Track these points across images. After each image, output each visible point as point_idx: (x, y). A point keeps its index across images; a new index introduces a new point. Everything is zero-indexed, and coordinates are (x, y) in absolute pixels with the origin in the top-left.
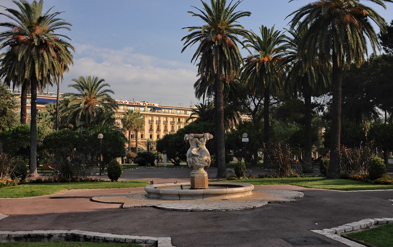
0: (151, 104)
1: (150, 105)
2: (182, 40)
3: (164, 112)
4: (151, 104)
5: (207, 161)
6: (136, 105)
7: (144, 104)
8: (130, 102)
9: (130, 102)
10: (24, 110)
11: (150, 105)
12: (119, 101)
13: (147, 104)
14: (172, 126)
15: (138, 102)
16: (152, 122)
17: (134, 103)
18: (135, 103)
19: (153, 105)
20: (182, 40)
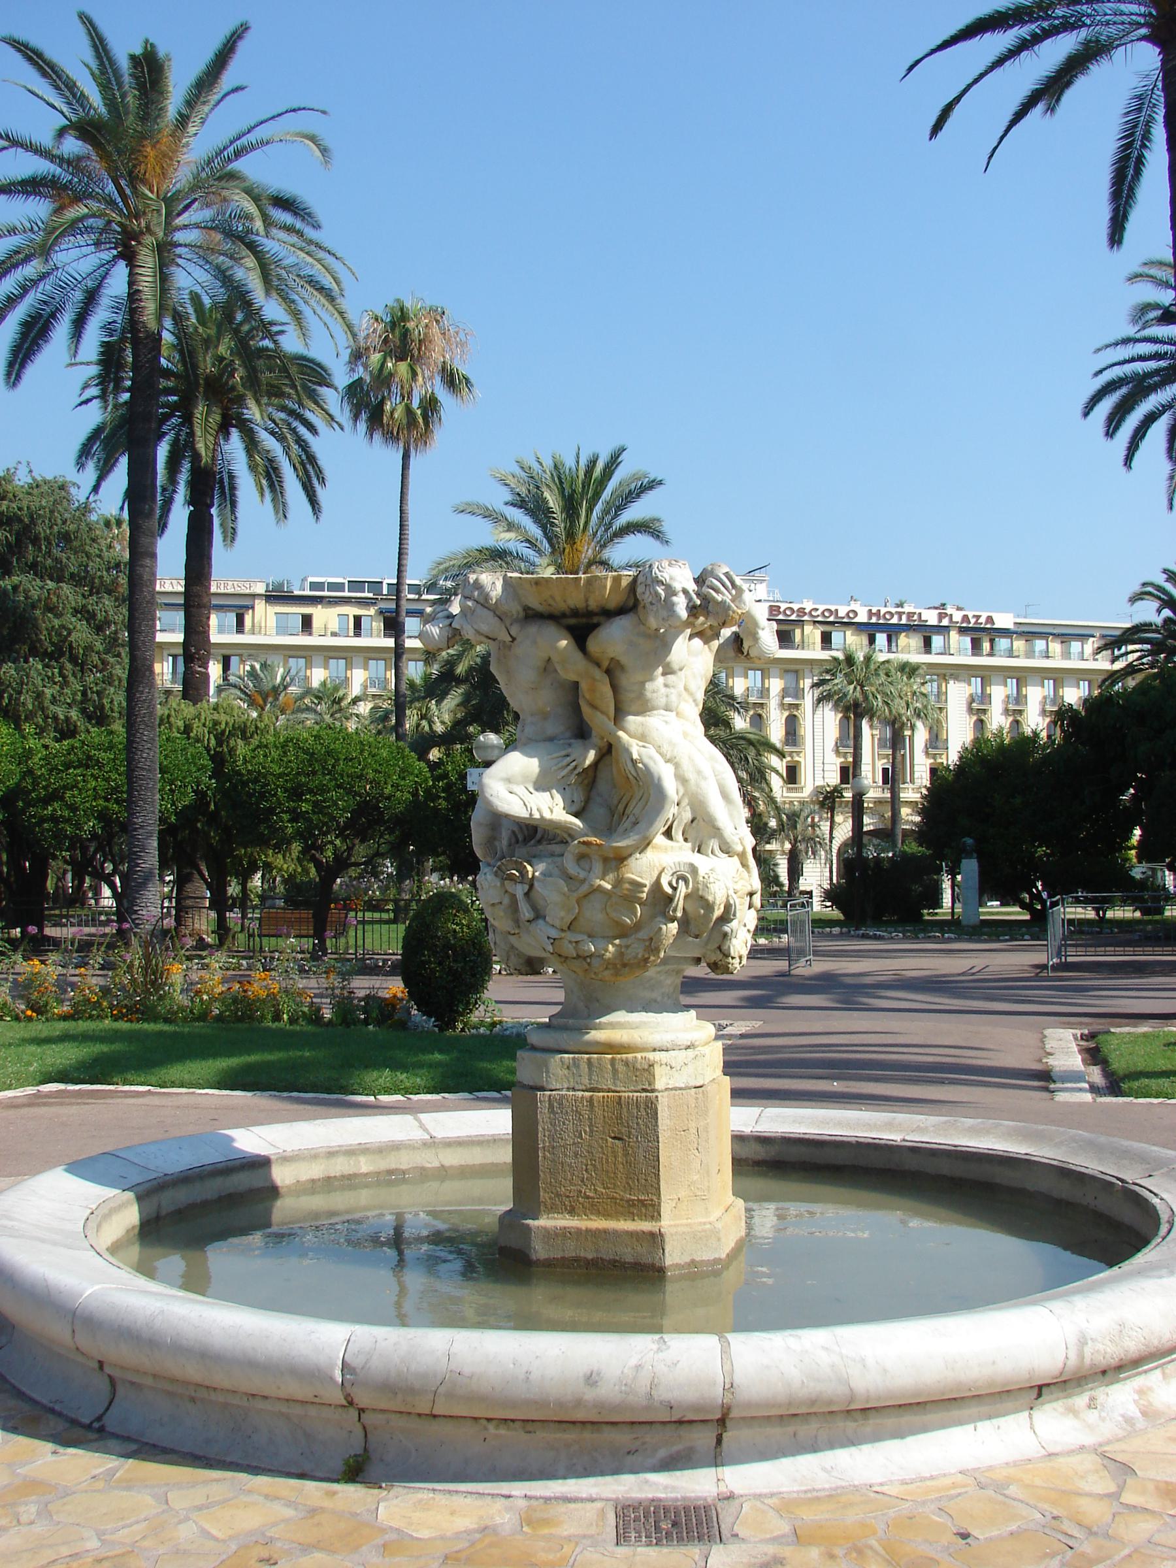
0: (978, 617)
1: (973, 621)
2: (1088, 410)
3: (1011, 654)
4: (978, 617)
5: (670, 899)
6: (904, 621)
7: (941, 616)
8: (874, 611)
9: (874, 611)
10: (199, 633)
11: (973, 621)
12: (822, 608)
13: (957, 616)
14: (975, 718)
15: (912, 610)
16: (982, 703)
17: (892, 615)
18: (900, 614)
19: (990, 619)
20: (1088, 410)
